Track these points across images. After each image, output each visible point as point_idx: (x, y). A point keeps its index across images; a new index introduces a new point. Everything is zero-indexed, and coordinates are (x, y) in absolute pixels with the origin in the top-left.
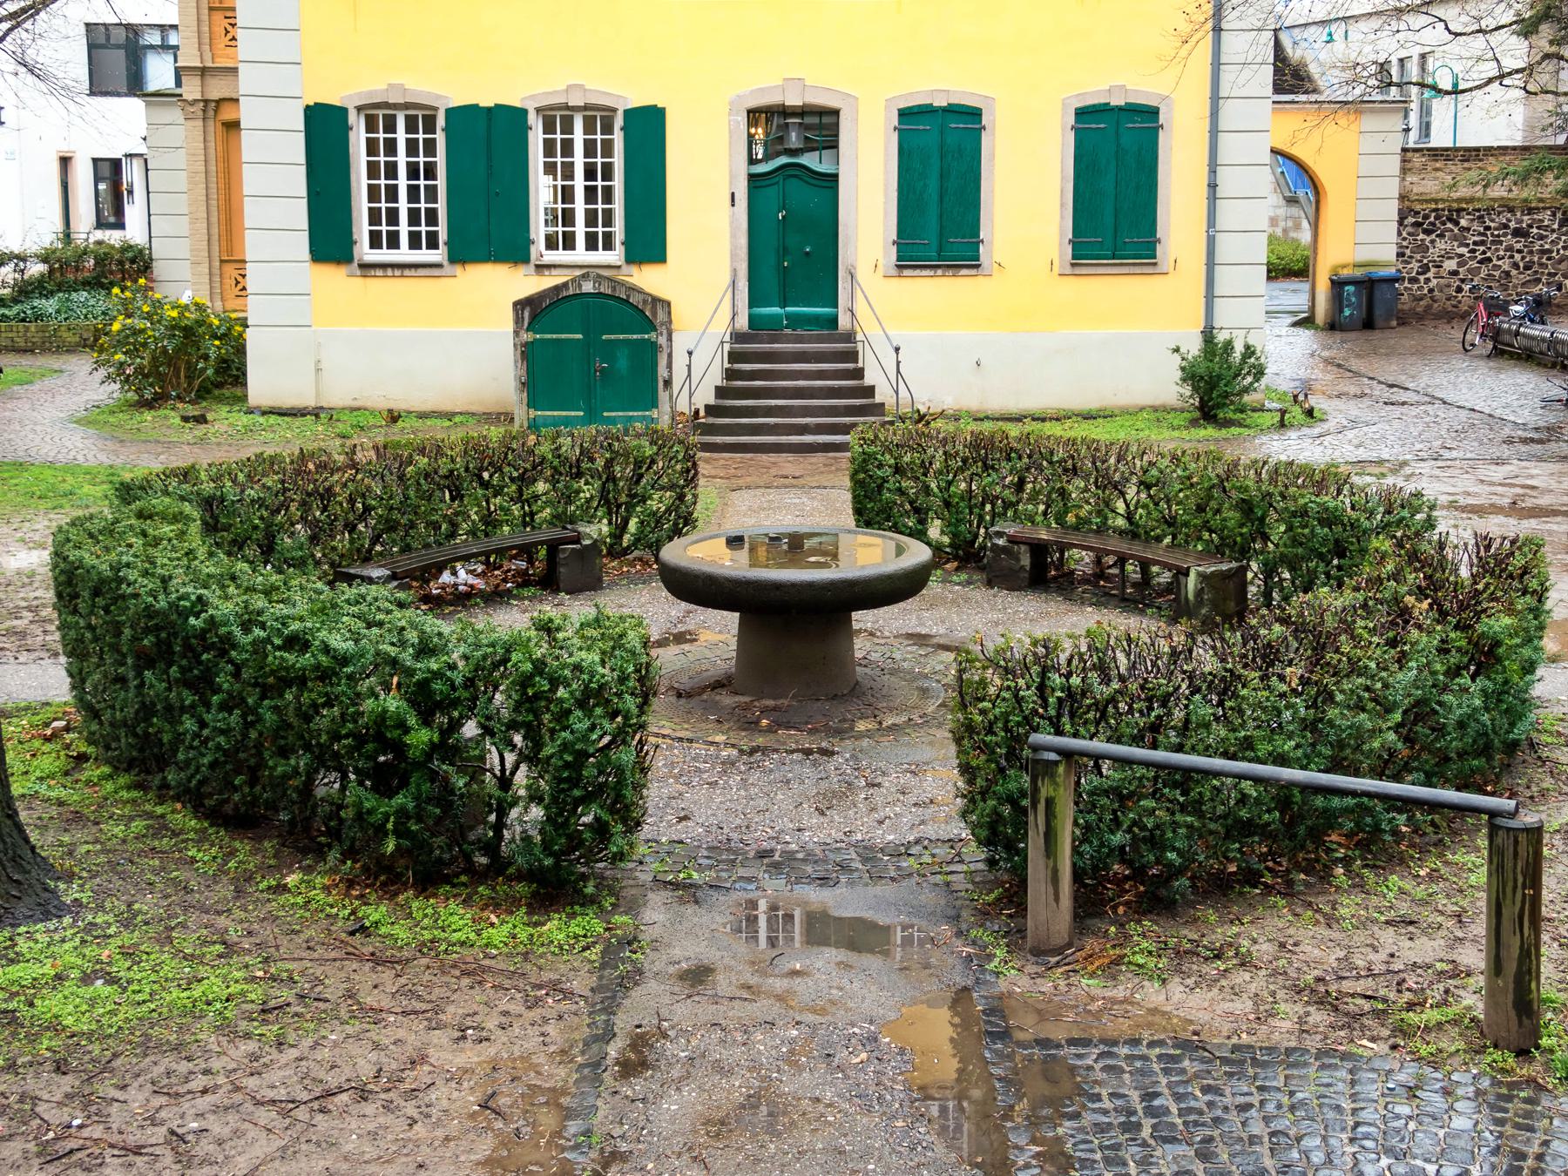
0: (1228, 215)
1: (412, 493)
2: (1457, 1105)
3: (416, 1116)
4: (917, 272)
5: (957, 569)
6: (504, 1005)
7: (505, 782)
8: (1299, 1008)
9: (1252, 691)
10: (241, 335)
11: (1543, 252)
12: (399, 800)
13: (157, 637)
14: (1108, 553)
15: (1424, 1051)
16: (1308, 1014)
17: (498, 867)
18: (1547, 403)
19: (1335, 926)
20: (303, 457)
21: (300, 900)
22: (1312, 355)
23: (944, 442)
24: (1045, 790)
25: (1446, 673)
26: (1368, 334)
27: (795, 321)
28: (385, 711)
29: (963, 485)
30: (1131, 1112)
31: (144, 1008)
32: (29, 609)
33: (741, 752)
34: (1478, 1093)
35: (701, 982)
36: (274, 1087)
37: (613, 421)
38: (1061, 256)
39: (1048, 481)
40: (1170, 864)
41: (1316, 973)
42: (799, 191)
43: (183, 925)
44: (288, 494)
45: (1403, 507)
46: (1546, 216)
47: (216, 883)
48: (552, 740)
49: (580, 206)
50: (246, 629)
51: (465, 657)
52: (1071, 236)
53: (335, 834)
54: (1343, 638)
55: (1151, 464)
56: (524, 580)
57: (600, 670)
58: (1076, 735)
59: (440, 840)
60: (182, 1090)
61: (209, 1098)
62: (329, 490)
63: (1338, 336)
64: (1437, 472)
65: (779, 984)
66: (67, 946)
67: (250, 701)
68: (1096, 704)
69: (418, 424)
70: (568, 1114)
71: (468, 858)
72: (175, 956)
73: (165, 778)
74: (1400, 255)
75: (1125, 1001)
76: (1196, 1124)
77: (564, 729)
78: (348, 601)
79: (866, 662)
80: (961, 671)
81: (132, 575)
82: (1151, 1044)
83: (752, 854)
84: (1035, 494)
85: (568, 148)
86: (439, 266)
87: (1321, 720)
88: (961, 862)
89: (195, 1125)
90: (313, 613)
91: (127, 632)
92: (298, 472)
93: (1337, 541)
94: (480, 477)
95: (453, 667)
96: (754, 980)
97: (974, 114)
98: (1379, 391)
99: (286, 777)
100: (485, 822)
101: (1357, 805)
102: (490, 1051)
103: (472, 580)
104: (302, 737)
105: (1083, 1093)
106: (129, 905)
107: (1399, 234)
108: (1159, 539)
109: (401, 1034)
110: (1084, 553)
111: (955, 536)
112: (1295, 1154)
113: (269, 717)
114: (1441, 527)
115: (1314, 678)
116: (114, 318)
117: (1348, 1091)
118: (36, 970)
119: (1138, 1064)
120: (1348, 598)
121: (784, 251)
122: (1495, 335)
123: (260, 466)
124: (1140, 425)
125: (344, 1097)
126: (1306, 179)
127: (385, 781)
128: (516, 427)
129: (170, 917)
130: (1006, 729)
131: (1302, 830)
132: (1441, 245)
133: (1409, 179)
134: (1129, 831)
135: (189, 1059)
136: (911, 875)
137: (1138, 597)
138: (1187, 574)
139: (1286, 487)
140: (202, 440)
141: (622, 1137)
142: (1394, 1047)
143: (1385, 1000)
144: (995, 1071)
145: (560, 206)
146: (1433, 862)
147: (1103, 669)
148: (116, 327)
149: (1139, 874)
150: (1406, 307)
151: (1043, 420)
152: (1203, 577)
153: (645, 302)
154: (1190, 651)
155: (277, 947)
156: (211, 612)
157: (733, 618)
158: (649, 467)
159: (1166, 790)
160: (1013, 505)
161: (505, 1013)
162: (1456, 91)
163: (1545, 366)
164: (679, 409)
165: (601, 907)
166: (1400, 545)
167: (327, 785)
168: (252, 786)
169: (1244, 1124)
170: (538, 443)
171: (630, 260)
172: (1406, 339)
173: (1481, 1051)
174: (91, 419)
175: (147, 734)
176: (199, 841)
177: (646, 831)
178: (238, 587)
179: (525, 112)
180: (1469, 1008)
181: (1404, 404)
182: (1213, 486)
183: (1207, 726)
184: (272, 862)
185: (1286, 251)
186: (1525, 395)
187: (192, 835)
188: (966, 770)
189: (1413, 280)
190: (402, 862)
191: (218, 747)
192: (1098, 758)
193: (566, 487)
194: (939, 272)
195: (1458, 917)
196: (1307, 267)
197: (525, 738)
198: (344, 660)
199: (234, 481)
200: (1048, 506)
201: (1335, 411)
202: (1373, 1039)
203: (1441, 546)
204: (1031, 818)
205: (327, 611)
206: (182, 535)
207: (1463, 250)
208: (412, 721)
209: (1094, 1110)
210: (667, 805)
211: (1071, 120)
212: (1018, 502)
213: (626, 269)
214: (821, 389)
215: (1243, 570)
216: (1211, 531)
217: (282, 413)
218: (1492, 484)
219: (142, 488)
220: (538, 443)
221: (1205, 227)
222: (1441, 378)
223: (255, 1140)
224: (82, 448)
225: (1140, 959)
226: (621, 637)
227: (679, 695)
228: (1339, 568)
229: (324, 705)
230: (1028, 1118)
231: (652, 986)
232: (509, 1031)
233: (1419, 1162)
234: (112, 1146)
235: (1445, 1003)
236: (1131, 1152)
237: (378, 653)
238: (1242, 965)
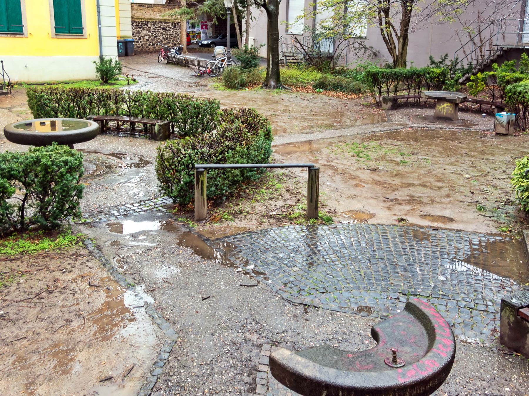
11: (170, 35)
38: (52, 32)
74: (133, 34)
122: (166, 57)
132: (144, 32)
133: (133, 12)
138: (155, 125)
142: (291, 223)
151: (51, 84)
152: (160, 126)
163: (183, 66)
172: (136, 59)
189: (137, 42)
194: (9, 36)
207: (150, 33)
221: (97, 24)
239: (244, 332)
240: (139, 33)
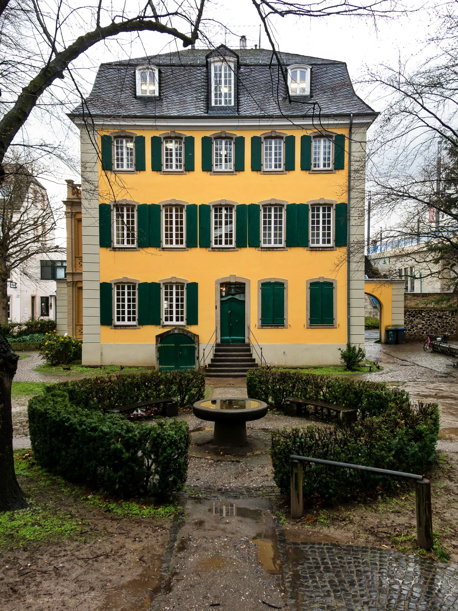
0: (354, 312)
6: (147, 531)
8: (366, 536)
11: (447, 323)
12: (120, 473)
16: (368, 537)
18: (448, 366)
20: (97, 379)
21: (92, 502)
23: (272, 375)
24: (295, 471)
27: (233, 341)
28: (117, 448)
30: (318, 563)
32: (19, 423)
33: (215, 461)
34: (415, 561)
36: (83, 554)
37: (182, 368)
43: (60, 510)
46: (447, 313)
49: (174, 309)
50: (80, 426)
56: (156, 413)
57: (175, 436)
58: (303, 456)
60: (58, 555)
61: (65, 558)
62: (104, 388)
63: (388, 346)
64: (414, 385)
65: (222, 526)
66: (28, 516)
69: (129, 370)
70: (163, 562)
74: (405, 323)
75: (318, 532)
76: (336, 567)
78: (108, 418)
79: (250, 436)
80: (273, 437)
81: (50, 412)
82: (324, 545)
85: (171, 294)
91: (48, 428)
92: (95, 383)
95: (135, 435)
96: (215, 525)
97: (282, 284)
98: (399, 361)
103: (142, 413)
105: (305, 558)
106: (45, 504)
109: (118, 539)
111: (276, 401)
113: (86, 450)
116: (46, 341)
118: (19, 523)
120: (381, 419)
123: (86, 381)
124: (330, 370)
125: (102, 557)
127: (116, 469)
128: (156, 370)
129: (56, 508)
132: (417, 320)
134: (319, 483)
135: (60, 547)
137: (327, 419)
138: (340, 412)
141: (177, 568)
142: (392, 547)
143: (390, 534)
144: (281, 551)
147: (312, 437)
148: (46, 343)
151: (303, 369)
155: (85, 516)
157: (213, 423)
161: (147, 534)
162: (421, 278)
169: (349, 567)
170: (161, 375)
173: (416, 549)
174: (38, 369)
177: (187, 483)
179: (160, 284)
180: (414, 537)
182: (346, 388)
183: (340, 454)
186: (441, 364)
188: (274, 465)
189: (409, 330)
198: (106, 434)
199: (78, 386)
201: (386, 367)
202: (386, 545)
205: (102, 421)
206: (64, 401)
207: (423, 322)
208: (124, 451)
209: (308, 563)
211: (309, 286)
213: (187, 326)
216: (347, 400)
218: (430, 389)
219: (53, 388)
223: (77, 569)
224: (37, 378)
225: (322, 520)
227: (198, 445)
229: (100, 447)
231: (187, 526)
233: (397, 579)
234: (38, 571)
235: (407, 535)
236: (317, 575)
237: (116, 432)
238: (351, 523)
240: (412, 321)
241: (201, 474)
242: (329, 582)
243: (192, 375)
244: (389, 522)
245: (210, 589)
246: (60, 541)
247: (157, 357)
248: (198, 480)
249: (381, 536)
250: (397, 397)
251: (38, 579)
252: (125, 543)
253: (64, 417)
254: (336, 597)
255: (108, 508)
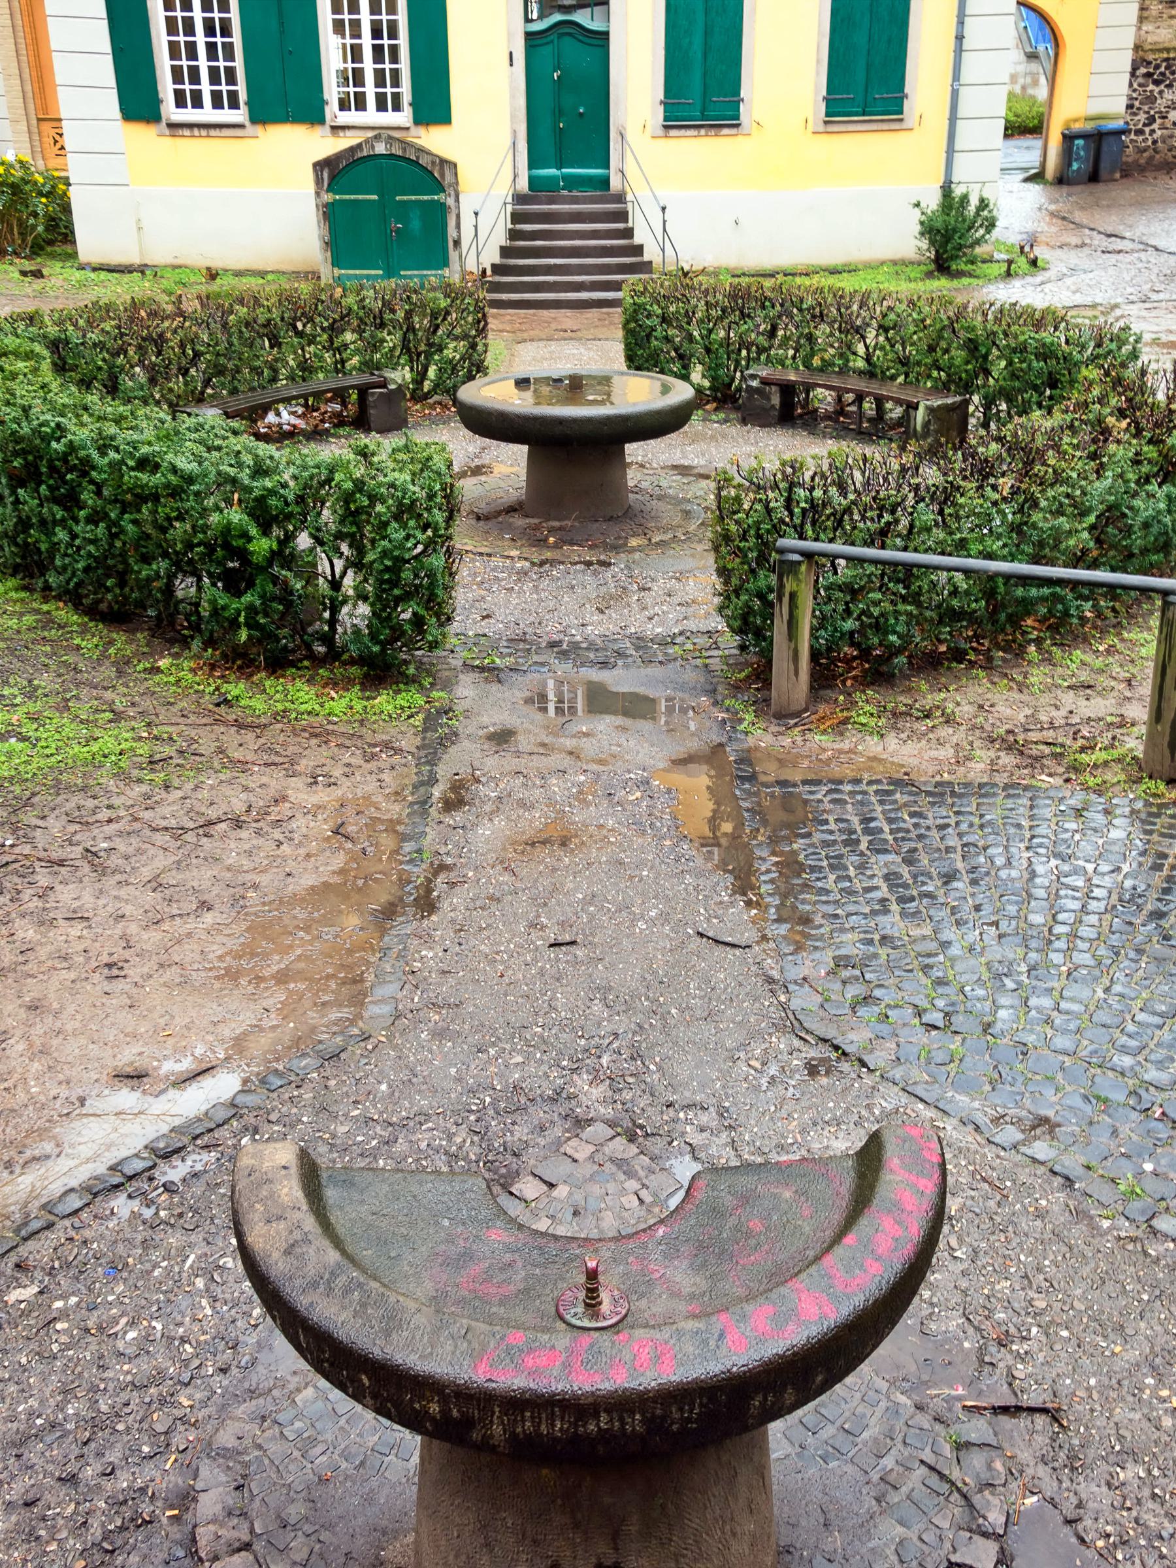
1: (235, 341)
2: (1115, 822)
3: (282, 839)
4: (682, 132)
5: (716, 409)
7: (336, 585)
8: (992, 754)
9: (969, 499)
10: (65, 194)
12: (247, 598)
13: (25, 459)
14: (848, 391)
15: (1091, 782)
16: (998, 758)
17: (334, 655)
19: (1025, 691)
20: (135, 305)
21: (172, 679)
22: (1040, 209)
23: (706, 293)
24: (790, 585)
25: (1137, 482)
26: (1093, 187)
27: (573, 183)
28: (229, 523)
29: (722, 334)
31: (53, 759)
33: (533, 564)
34: (1133, 812)
35: (506, 742)
36: (165, 818)
38: (815, 114)
39: (797, 328)
40: (892, 644)
41: (1007, 727)
42: (570, 47)
43: (77, 698)
44: (126, 338)
45: (1111, 340)
47: (100, 665)
48: (374, 548)
49: (368, 66)
51: (295, 477)
52: (824, 93)
53: (196, 628)
54: (1051, 453)
55: (890, 308)
56: (340, 421)
58: (816, 540)
59: (285, 632)
61: (114, 826)
63: (1065, 189)
64: (1144, 313)
65: (569, 743)
67: (113, 515)
68: (833, 514)
69: (234, 281)
70: (404, 838)
71: (308, 647)
72: (73, 721)
73: (46, 581)
74: (1130, 107)
75: (850, 751)
76: (903, 839)
77: (384, 538)
78: (188, 429)
79: (637, 490)
82: (870, 783)
83: (544, 644)
84: (786, 339)
86: (241, 126)
87: (1026, 523)
88: (718, 648)
89: (105, 845)
90: (158, 438)
92: (132, 319)
93: (1050, 373)
94: (295, 327)
95: (284, 486)
98: (1099, 241)
99: (149, 580)
100: (320, 618)
101: (1053, 594)
102: (338, 792)
103: (294, 421)
104: (160, 546)
106: (30, 681)
107: (1131, 85)
108: (893, 378)
109: (265, 780)
110: (827, 393)
111: (714, 379)
112: (982, 859)
114: (1144, 358)
115: (1023, 486)
117: (1028, 813)
119: (859, 797)
120: (1058, 418)
121: (559, 113)
123: (99, 311)
124: (880, 278)
125: (223, 826)
126: (1048, 30)
127: (234, 583)
129: (64, 691)
130: (759, 536)
131: (1003, 617)
133: (1144, 28)
134: (858, 618)
135: (94, 797)
136: (675, 659)
138: (916, 408)
139: (1009, 326)
140: (42, 293)
141: (447, 854)
142: (1067, 780)
143: (1062, 746)
144: (744, 804)
145: (350, 65)
146: (1112, 640)
149: (865, 654)
150: (1130, 160)
151: (794, 275)
152: (931, 410)
153: (433, 163)
154: (917, 469)
155: (157, 715)
156: (70, 437)
158: (445, 319)
159: (891, 585)
160: (765, 350)
161: (348, 765)
164: (468, 269)
165: (421, 686)
166: (1107, 374)
167: (185, 588)
168: (122, 588)
169: (942, 839)
171: (418, 121)
173: (1139, 780)
175: (26, 544)
176: (82, 633)
177: (455, 627)
178: (91, 415)
180: (1132, 750)
181: (1120, 252)
184: (145, 650)
185: (1022, 108)
187: (75, 628)
189: (1140, 132)
190: (254, 650)
191: (90, 555)
192: (834, 557)
193: (372, 336)
194: (703, 132)
195: (1129, 682)
196: (1041, 122)
197: (350, 546)
198: (190, 479)
199: (75, 325)
200: (797, 350)
202: (1050, 775)
203: (1143, 372)
204: (777, 609)
205: (171, 437)
206: (35, 371)
208: (253, 531)
210: (472, 606)
212: (770, 348)
213: (415, 131)
214: (595, 248)
215: (967, 403)
216: (939, 369)
217: (111, 270)
220: (344, 295)
222: (1156, 227)
225: (863, 720)
226: (429, 459)
227: (478, 518)
228: (1051, 398)
229: (177, 519)
230: (769, 837)
231: (466, 744)
232: (352, 778)
233: (1081, 863)
234: (39, 860)
235: (1112, 746)
237: (219, 473)
238: (947, 722)
239: (573, 1071)
240: (1151, 99)
241: (495, 599)
242: (886, 878)
243: (446, 296)
244: (1059, 716)
245: (545, 904)
246: (91, 782)
247: (322, 238)
248: (488, 616)
249: (1034, 752)
250: (1100, 351)
251: (43, 878)
252: (286, 788)
253: (44, 424)
254: (903, 914)
255: (221, 694)
